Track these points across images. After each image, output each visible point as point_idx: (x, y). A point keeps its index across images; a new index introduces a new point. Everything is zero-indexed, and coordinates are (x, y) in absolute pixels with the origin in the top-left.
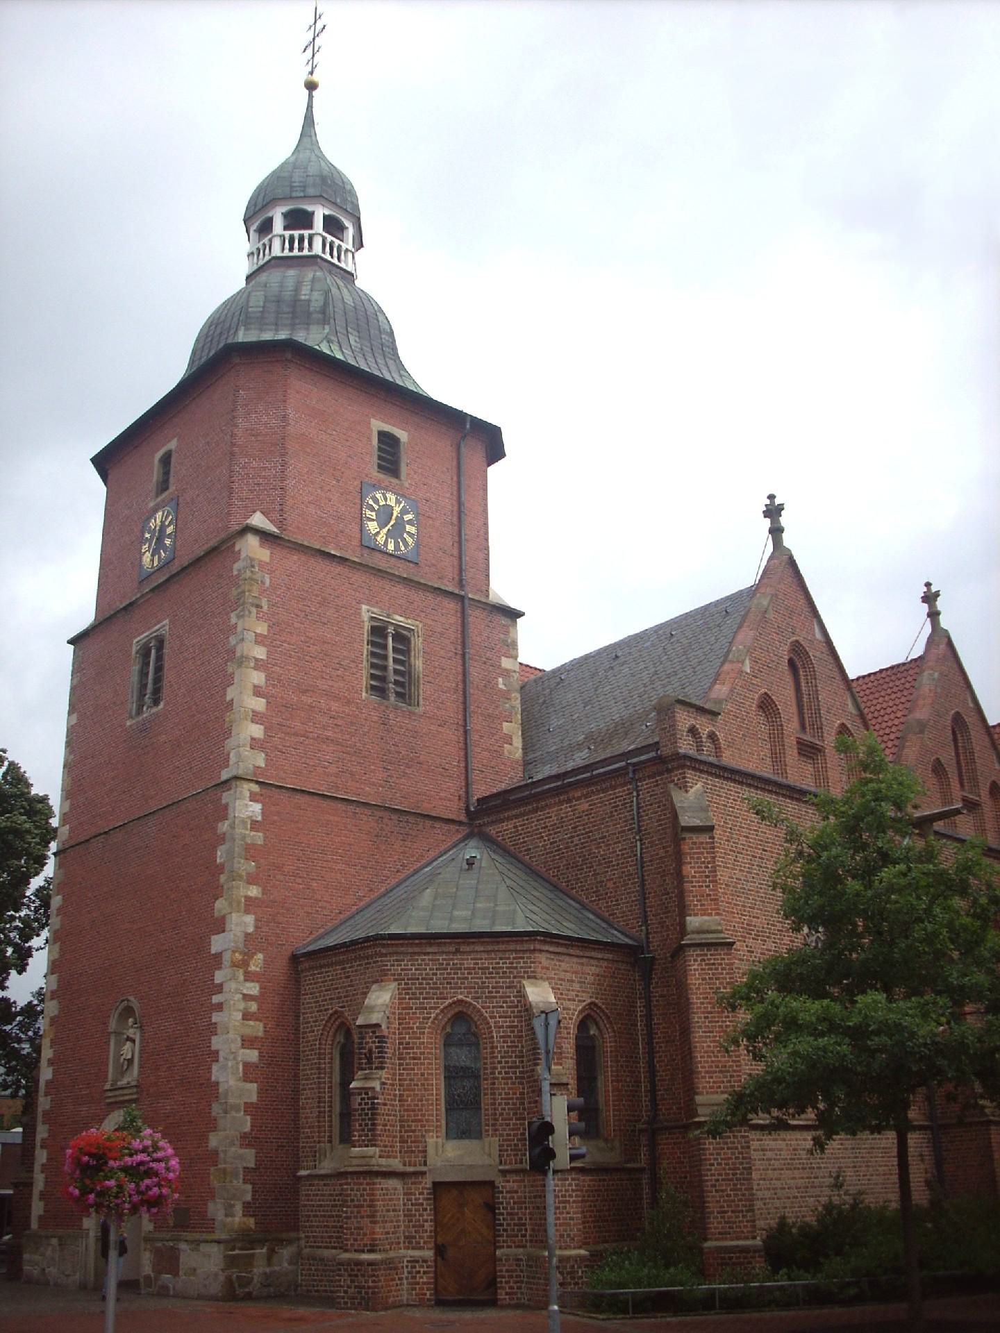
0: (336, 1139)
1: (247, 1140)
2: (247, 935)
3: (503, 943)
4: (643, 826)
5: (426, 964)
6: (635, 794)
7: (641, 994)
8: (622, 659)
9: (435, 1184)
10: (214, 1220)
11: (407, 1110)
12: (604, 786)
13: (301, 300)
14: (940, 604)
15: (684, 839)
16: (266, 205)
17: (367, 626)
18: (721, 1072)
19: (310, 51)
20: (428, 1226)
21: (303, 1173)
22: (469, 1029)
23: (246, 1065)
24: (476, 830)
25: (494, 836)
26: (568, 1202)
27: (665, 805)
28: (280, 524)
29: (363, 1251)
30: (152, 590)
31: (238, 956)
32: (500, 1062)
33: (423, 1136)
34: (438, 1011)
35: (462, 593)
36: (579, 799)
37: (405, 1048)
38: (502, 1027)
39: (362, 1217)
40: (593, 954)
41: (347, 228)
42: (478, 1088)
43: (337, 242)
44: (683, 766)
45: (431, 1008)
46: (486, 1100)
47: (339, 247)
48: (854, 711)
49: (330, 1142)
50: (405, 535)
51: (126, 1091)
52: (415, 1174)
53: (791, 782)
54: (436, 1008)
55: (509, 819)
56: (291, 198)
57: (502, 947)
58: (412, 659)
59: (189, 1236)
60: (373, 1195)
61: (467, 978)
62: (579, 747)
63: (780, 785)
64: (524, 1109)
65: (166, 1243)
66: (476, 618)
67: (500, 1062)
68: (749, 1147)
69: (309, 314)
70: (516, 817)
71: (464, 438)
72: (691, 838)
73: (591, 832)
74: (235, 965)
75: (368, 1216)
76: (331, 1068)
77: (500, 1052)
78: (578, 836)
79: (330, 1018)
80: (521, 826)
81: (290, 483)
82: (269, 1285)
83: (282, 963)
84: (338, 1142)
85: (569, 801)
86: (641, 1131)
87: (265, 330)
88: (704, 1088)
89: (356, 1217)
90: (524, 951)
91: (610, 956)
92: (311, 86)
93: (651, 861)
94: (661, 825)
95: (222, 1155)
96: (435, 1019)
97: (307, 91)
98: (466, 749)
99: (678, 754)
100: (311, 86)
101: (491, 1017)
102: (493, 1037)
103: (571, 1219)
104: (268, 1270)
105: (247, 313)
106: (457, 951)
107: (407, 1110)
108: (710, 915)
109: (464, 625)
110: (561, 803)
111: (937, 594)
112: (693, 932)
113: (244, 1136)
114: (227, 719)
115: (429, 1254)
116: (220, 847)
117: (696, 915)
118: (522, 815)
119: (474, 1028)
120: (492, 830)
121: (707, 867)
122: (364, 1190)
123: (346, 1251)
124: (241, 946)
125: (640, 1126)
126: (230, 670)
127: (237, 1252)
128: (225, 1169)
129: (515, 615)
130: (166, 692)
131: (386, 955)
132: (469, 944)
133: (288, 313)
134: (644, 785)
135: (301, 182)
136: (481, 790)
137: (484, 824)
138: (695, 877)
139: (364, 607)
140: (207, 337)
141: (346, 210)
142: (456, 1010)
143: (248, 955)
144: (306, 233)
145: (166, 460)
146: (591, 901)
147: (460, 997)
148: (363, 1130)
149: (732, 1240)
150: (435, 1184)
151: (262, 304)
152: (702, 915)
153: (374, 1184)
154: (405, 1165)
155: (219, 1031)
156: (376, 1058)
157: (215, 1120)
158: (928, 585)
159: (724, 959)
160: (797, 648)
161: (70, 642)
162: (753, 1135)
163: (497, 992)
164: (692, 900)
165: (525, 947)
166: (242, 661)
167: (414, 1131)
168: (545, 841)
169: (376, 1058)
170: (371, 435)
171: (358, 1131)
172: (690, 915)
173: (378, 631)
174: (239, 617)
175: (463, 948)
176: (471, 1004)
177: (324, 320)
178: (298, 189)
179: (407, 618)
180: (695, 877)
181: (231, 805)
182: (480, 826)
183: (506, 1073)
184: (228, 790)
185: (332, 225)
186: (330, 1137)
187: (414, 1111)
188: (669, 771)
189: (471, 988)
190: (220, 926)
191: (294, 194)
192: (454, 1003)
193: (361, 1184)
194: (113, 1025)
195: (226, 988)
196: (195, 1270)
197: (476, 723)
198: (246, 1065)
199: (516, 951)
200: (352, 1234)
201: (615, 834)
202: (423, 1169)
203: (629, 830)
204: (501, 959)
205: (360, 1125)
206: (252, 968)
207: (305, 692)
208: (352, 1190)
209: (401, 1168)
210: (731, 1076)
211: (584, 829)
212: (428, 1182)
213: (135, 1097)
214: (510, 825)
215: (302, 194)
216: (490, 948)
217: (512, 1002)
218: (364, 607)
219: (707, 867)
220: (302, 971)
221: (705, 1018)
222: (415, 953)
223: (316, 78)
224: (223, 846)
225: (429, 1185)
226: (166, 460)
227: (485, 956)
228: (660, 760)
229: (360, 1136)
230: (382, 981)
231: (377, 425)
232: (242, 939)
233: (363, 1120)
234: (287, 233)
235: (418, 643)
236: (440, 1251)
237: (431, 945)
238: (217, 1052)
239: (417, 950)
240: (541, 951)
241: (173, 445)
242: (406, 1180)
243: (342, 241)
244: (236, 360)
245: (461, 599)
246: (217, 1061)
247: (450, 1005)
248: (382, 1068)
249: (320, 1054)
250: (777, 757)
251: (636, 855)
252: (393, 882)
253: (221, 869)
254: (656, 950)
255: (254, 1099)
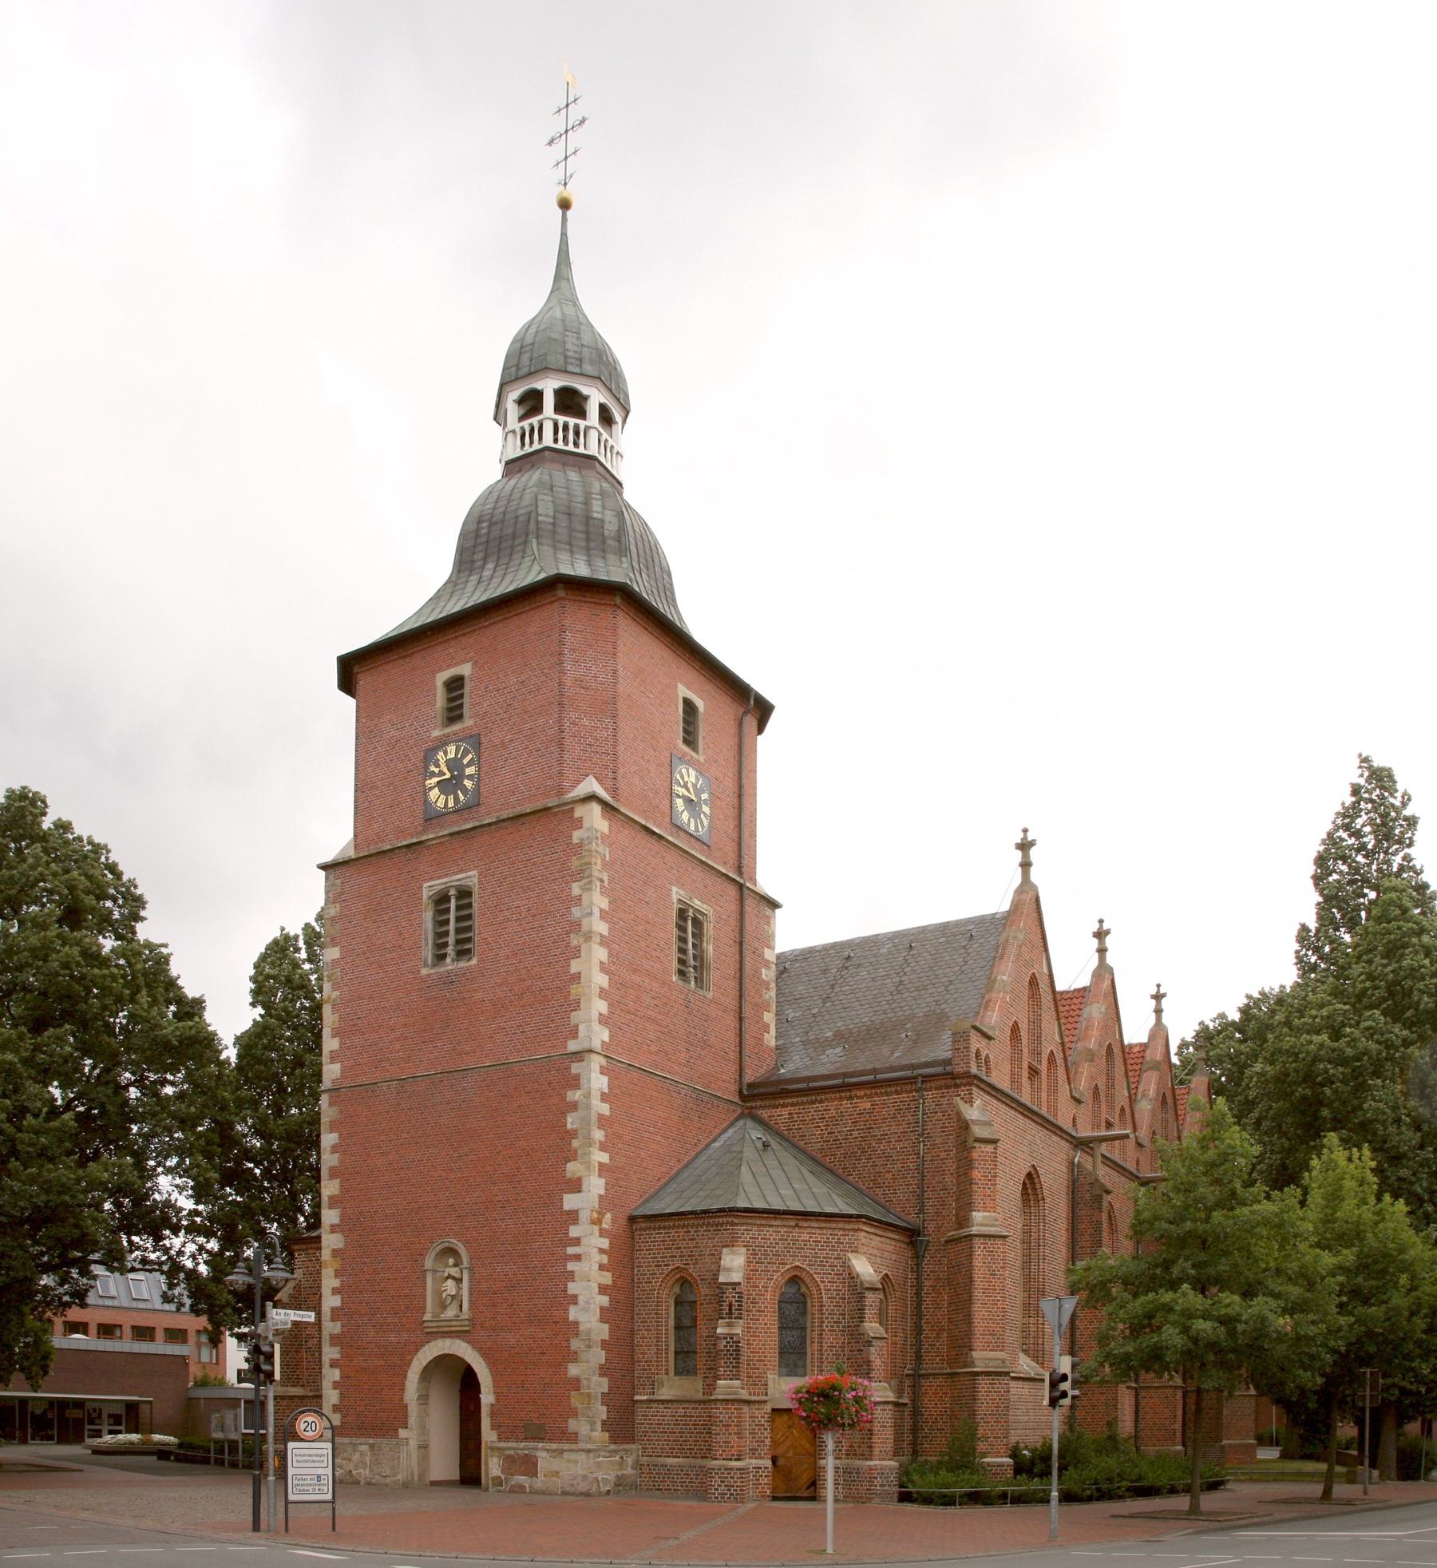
0: (672, 1373)
1: (604, 1371)
2: (600, 1196)
3: (834, 1221)
4: (926, 1130)
5: (771, 1234)
6: (921, 1102)
7: (912, 1268)
8: (855, 961)
9: (773, 1410)
10: (576, 1434)
11: (753, 1352)
12: (889, 1090)
13: (595, 519)
14: (1109, 941)
15: (975, 1147)
16: (534, 373)
17: (676, 907)
18: (990, 1335)
19: (559, 146)
20: (768, 1442)
21: (637, 1398)
22: (799, 1289)
23: (602, 1309)
24: (746, 1111)
25: (766, 1118)
26: (886, 1427)
27: (949, 1115)
28: (614, 792)
29: (731, 1460)
30: (451, 835)
31: (595, 1215)
32: (827, 1318)
33: (765, 1373)
34: (779, 1274)
35: (742, 881)
36: (861, 1097)
37: (752, 1303)
38: (830, 1290)
39: (730, 1434)
40: (890, 1235)
41: (617, 423)
42: (804, 1337)
43: (605, 436)
44: (970, 1084)
45: (773, 1271)
46: (812, 1349)
47: (577, 427)
48: (1059, 1040)
49: (667, 1374)
50: (702, 816)
51: (454, 1323)
52: (759, 1402)
53: (1023, 1100)
54: (778, 1272)
55: (784, 1106)
56: (566, 371)
57: (834, 1225)
58: (705, 944)
59: (549, 1446)
60: (740, 1417)
61: (803, 1249)
62: (829, 1044)
63: (1013, 1100)
64: (844, 1355)
65: (519, 1451)
66: (750, 903)
67: (827, 1318)
68: (1009, 1392)
69: (604, 540)
70: (793, 1105)
71: (745, 713)
72: (980, 1148)
73: (872, 1128)
74: (593, 1222)
75: (735, 1434)
76: (668, 1314)
77: (827, 1310)
78: (858, 1130)
79: (670, 1273)
80: (796, 1113)
81: (621, 748)
82: (620, 1485)
83: (623, 1222)
84: (673, 1373)
85: (850, 1098)
86: (907, 1375)
87: (560, 549)
88: (978, 1346)
89: (724, 1434)
90: (849, 1230)
91: (897, 1237)
92: (565, 205)
93: (931, 1160)
94: (943, 1132)
95: (585, 1382)
96: (776, 1280)
97: (560, 212)
98: (741, 1035)
99: (969, 1073)
100: (565, 205)
101: (822, 1282)
102: (822, 1298)
103: (887, 1439)
104: (619, 1473)
105: (538, 522)
106: (797, 1226)
107: (753, 1352)
108: (989, 1211)
109: (742, 913)
110: (841, 1099)
111: (1108, 932)
112: (977, 1225)
113: (601, 1367)
114: (573, 991)
115: (769, 1463)
116: (572, 1114)
117: (979, 1211)
118: (803, 1103)
119: (803, 1289)
120: (764, 1114)
121: (990, 1173)
122: (732, 1413)
123: (716, 1459)
124: (597, 1206)
125: (906, 1372)
126: (575, 942)
127: (601, 1459)
128: (589, 1394)
129: (774, 905)
130: (477, 945)
131: (737, 1224)
132: (806, 1220)
133: (581, 532)
134: (929, 1095)
135: (576, 352)
136: (750, 1076)
137: (756, 1107)
138: (980, 1180)
139: (674, 889)
140: (477, 536)
141: (618, 400)
142: (792, 1274)
143: (601, 1214)
144: (582, 424)
145: (455, 685)
146: (868, 1188)
147: (797, 1264)
148: (728, 1367)
149: (992, 1457)
150: (773, 1410)
151: (552, 514)
152: (984, 1211)
153: (741, 1409)
154: (750, 1394)
155: (576, 1278)
156: (736, 1310)
157: (576, 1353)
158: (1101, 921)
159: (999, 1248)
160: (1033, 977)
161: (324, 867)
162: (1013, 1384)
163: (827, 1262)
164: (977, 1197)
165: (851, 1226)
166: (588, 937)
167: (758, 1369)
168: (822, 1130)
169: (736, 1310)
170: (677, 700)
171: (723, 1367)
172: (975, 1211)
173: (682, 914)
174: (583, 889)
175: (801, 1224)
176: (805, 1270)
177: (620, 549)
178: (573, 361)
179: (703, 903)
180: (980, 1180)
181: (582, 1076)
182: (752, 1108)
183: (832, 1326)
184: (579, 1061)
185: (606, 418)
186: (667, 1370)
187: (758, 1352)
188: (957, 1086)
189: (806, 1257)
190: (576, 1186)
191: (570, 368)
192: (792, 1268)
193: (730, 1409)
194: (429, 1263)
195: (584, 1241)
196: (558, 1473)
197: (748, 1011)
198: (602, 1309)
199: (844, 1230)
200: (721, 1446)
201: (896, 1133)
202: (764, 1398)
203: (911, 1132)
204: (831, 1235)
205: (725, 1363)
206: (604, 1226)
207: (635, 971)
208: (721, 1413)
209: (747, 1397)
210: (998, 1339)
211: (865, 1125)
212: (768, 1408)
213: (467, 1328)
214: (785, 1112)
215: (577, 370)
216: (823, 1225)
217: (838, 1270)
218: (674, 889)
219: (990, 1173)
220: (636, 1230)
221: (984, 1293)
222: (761, 1225)
223: (571, 192)
224: (576, 1113)
225: (769, 1411)
226: (455, 685)
227: (818, 1231)
228: (952, 1076)
229: (725, 1371)
230: (733, 1246)
231: (683, 691)
232: (597, 1200)
233: (728, 1359)
234: (561, 419)
235: (709, 929)
236: (774, 1460)
237: (775, 1219)
238: (576, 1296)
239: (764, 1222)
240: (862, 1230)
241: (465, 670)
242: (752, 1406)
243: (611, 437)
244: (561, 593)
245: (741, 887)
246: (576, 1304)
247: (789, 1269)
248: (741, 1318)
249: (658, 1302)
250: (1014, 1078)
251: (919, 1154)
252: (693, 1154)
253: (573, 1134)
254: (929, 1235)
255: (607, 1337)
